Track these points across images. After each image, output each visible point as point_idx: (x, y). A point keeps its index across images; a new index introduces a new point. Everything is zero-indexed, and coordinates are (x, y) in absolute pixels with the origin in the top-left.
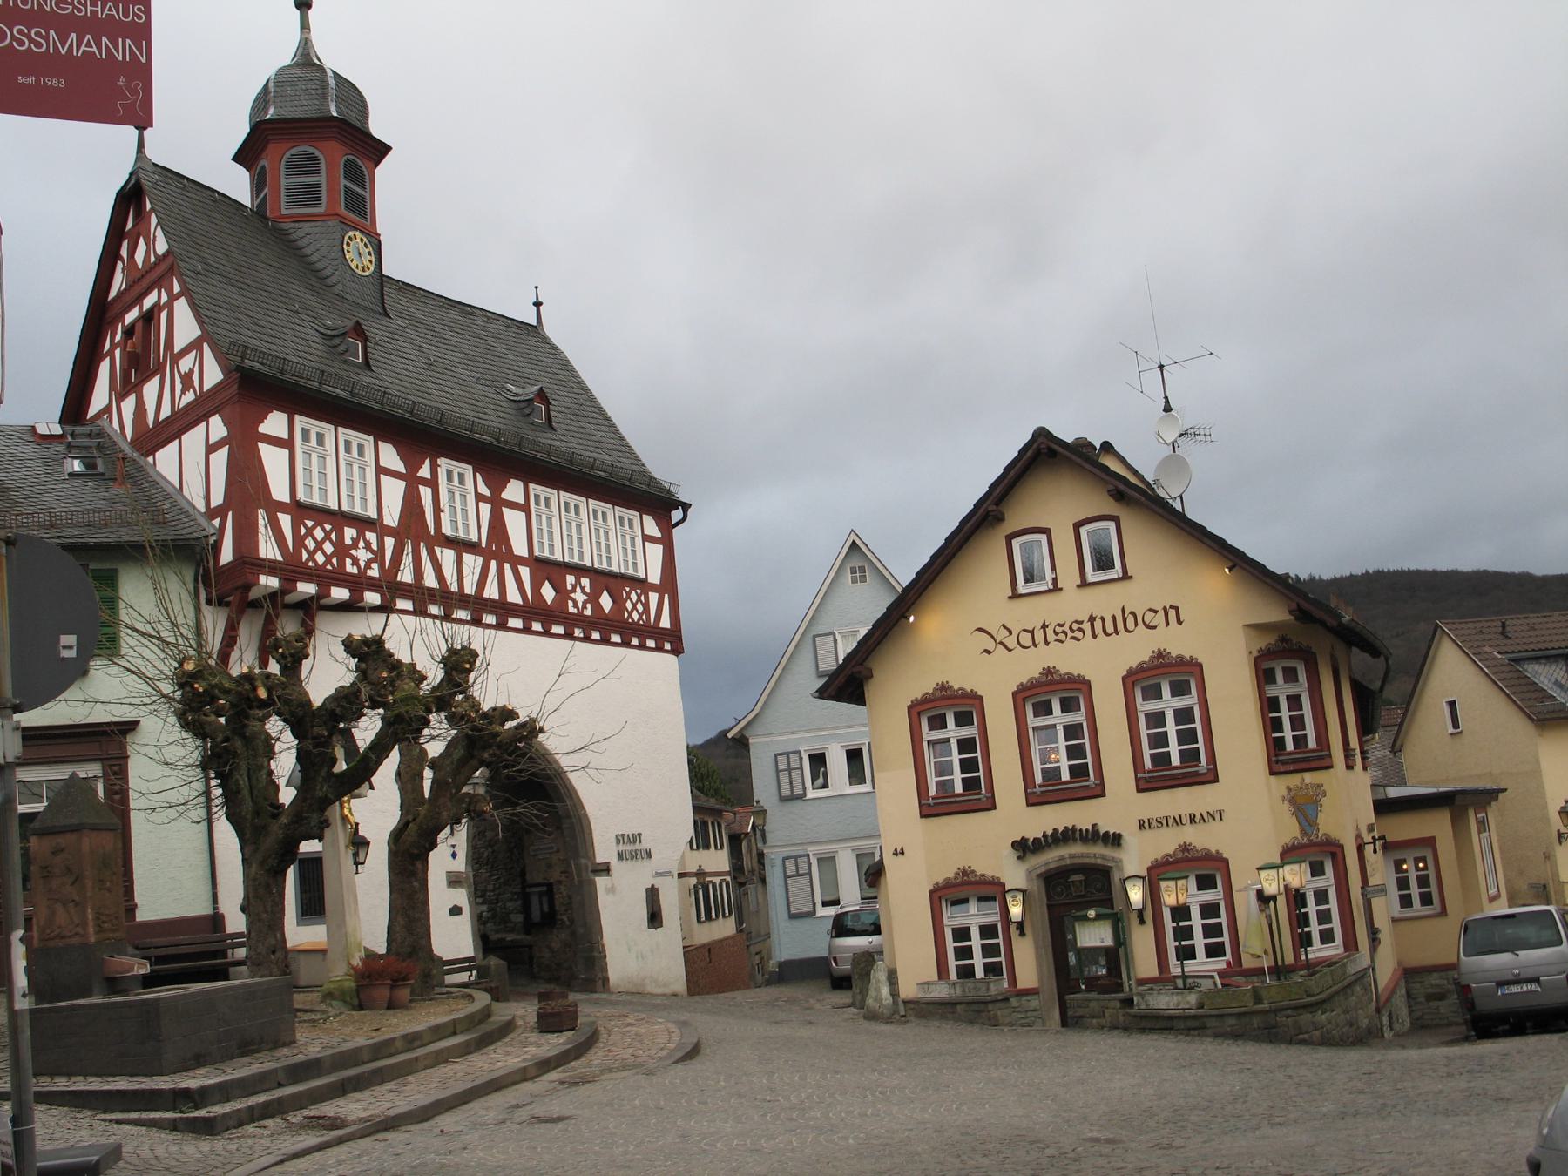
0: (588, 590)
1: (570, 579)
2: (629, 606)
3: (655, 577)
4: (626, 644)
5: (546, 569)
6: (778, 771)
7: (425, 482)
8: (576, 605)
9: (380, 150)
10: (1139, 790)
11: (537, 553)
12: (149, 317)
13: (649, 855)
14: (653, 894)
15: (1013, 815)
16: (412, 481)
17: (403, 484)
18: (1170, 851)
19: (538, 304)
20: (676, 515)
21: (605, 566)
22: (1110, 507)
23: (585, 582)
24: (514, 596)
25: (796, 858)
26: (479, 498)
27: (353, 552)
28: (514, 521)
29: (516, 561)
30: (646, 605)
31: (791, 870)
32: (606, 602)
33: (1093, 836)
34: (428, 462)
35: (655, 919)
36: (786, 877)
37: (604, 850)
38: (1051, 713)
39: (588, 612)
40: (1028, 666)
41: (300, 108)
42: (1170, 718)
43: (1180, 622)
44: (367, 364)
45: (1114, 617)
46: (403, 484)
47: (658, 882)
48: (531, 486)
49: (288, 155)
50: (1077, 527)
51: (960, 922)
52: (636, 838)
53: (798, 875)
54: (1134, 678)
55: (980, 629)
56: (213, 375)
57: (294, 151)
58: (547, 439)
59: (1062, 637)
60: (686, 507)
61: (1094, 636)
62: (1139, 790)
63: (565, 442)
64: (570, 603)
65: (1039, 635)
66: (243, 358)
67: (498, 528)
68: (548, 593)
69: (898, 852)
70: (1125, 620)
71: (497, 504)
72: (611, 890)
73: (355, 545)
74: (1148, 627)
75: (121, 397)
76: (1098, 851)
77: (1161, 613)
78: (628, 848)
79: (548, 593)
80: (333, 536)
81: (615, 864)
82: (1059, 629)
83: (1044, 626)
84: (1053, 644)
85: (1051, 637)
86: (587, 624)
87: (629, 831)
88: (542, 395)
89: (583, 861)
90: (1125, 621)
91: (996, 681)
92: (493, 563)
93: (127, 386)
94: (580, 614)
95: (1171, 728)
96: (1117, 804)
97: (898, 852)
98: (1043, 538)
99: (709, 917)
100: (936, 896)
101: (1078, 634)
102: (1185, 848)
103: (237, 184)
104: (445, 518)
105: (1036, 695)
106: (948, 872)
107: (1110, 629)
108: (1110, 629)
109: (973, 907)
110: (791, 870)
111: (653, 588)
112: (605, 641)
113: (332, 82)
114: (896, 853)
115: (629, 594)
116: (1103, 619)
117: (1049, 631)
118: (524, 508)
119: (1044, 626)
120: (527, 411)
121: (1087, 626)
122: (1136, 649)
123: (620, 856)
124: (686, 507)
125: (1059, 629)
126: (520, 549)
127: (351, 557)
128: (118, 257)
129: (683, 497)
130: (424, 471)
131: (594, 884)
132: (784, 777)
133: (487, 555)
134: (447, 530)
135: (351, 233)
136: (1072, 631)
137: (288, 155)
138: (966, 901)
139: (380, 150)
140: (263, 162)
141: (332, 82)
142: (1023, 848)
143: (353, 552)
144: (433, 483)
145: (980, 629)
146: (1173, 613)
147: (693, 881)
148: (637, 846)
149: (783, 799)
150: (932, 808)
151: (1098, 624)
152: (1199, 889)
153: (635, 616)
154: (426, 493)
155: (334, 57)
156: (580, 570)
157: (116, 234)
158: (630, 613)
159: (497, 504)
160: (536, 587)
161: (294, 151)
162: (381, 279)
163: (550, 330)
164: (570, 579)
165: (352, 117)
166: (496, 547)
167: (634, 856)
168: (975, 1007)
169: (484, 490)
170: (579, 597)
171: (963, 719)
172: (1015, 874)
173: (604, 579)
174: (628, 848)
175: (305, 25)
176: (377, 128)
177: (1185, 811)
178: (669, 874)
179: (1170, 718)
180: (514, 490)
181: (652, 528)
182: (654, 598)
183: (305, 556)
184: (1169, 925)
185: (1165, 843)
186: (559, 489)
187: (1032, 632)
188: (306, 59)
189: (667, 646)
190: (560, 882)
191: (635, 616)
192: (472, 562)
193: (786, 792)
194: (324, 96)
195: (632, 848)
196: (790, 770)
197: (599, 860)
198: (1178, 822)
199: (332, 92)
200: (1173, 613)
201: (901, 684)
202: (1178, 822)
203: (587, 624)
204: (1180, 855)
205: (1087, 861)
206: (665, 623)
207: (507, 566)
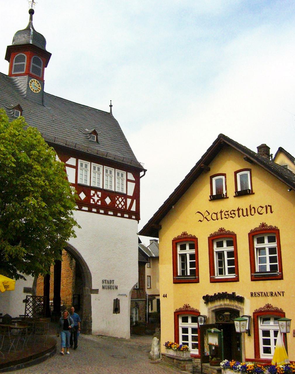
1: (93, 192)
2: (118, 202)
3: (130, 193)
8: (94, 200)
10: (252, 280)
11: (79, 182)
13: (117, 288)
15: (206, 287)
18: (262, 306)
19: (111, 106)
20: (142, 173)
22: (248, 165)
23: (99, 194)
27: (93, 197)
30: (126, 204)
32: (108, 201)
33: (233, 297)
35: (116, 310)
38: (223, 246)
40: (214, 227)
43: (271, 212)
45: (247, 209)
47: (119, 298)
48: (79, 160)
50: (236, 173)
51: (266, 328)
52: (112, 281)
54: (253, 234)
55: (198, 212)
59: (227, 216)
60: (145, 171)
61: (239, 216)
62: (252, 280)
63: (105, 148)
64: (92, 200)
65: (219, 215)
69: (165, 296)
70: (251, 210)
73: (94, 195)
74: (259, 213)
76: (234, 305)
77: (265, 208)
79: (83, 196)
80: (124, 200)
81: (100, 289)
82: (226, 213)
83: (221, 212)
84: (224, 219)
85: (223, 216)
87: (108, 279)
88: (95, 132)
90: (251, 211)
91: (202, 233)
94: (96, 204)
96: (244, 286)
97: (165, 296)
98: (223, 177)
100: (176, 314)
101: (233, 215)
102: (268, 306)
105: (217, 238)
106: (180, 306)
107: (245, 214)
108: (245, 214)
109: (272, 323)
111: (130, 197)
114: (164, 296)
115: (118, 199)
116: (242, 210)
117: (223, 214)
118: (76, 167)
119: (221, 212)
121: (236, 212)
122: (254, 222)
123: (103, 288)
124: (145, 171)
125: (226, 213)
129: (145, 168)
131: (90, 296)
135: (33, 80)
136: (231, 214)
137: (16, 56)
138: (268, 319)
142: (208, 299)
145: (198, 212)
146: (269, 208)
148: (112, 284)
150: (177, 280)
151: (241, 212)
152: (192, 322)
156: (96, 189)
158: (118, 205)
161: (18, 55)
163: (114, 114)
164: (93, 192)
167: (110, 288)
168: (178, 361)
172: (204, 310)
173: (106, 193)
174: (108, 285)
175: (31, 19)
176: (48, 49)
177: (269, 291)
180: (72, 161)
181: (131, 177)
182: (129, 201)
183: (116, 205)
184: (261, 338)
185: (260, 303)
186: (103, 165)
187: (217, 214)
195: (109, 285)
197: (94, 287)
198: (266, 295)
200: (269, 208)
201: (173, 230)
202: (266, 295)
203: (98, 208)
204: (266, 309)
205: (230, 307)
206: (133, 209)
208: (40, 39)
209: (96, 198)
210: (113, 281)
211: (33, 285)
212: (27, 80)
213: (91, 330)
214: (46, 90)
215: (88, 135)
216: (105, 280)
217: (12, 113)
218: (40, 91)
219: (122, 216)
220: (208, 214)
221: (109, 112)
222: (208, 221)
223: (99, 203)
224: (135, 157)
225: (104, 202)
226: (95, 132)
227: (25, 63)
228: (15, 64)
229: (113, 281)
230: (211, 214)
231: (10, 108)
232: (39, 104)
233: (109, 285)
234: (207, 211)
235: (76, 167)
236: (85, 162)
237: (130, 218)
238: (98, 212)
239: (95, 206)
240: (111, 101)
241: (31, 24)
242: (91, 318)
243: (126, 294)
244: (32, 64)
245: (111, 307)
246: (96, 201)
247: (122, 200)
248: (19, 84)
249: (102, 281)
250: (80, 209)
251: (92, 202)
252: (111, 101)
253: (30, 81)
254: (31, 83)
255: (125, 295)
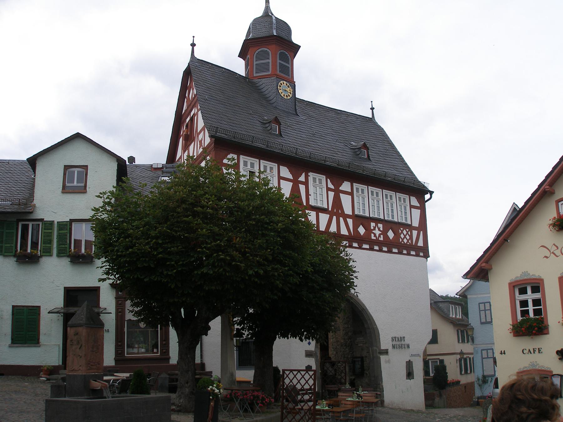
0: (381, 229)
1: (373, 225)
2: (402, 236)
3: (416, 224)
4: (400, 253)
5: (360, 220)
6: (480, 311)
7: (302, 183)
9: (296, 48)
11: (356, 213)
12: (192, 119)
13: (408, 346)
14: (409, 364)
16: (296, 183)
17: (291, 184)
19: (372, 109)
20: (427, 197)
21: (390, 219)
23: (380, 226)
24: (344, 231)
25: (487, 350)
26: (328, 189)
27: (374, 231)
28: (346, 200)
29: (346, 217)
30: (411, 236)
31: (485, 355)
32: (391, 234)
34: (304, 174)
35: (410, 375)
36: (483, 358)
37: (385, 343)
39: (381, 239)
41: (263, 33)
42: (530, 303)
44: (280, 134)
46: (291, 184)
47: (412, 359)
48: (354, 184)
49: (257, 52)
53: (488, 358)
55: (542, 246)
56: (208, 140)
57: (259, 50)
58: (369, 166)
60: (431, 193)
63: (376, 166)
64: (372, 235)
66: (216, 132)
67: (337, 202)
68: (362, 230)
71: (338, 192)
72: (389, 362)
73: (374, 229)
75: (184, 152)
78: (398, 343)
79: (362, 230)
80: (409, 233)
86: (381, 244)
87: (399, 335)
88: (365, 146)
89: (375, 348)
92: (335, 217)
93: (186, 148)
94: (377, 239)
95: (531, 308)
99: (466, 372)
103: (239, 67)
104: (311, 199)
110: (485, 355)
111: (415, 228)
112: (390, 251)
113: (274, 21)
114: (501, 353)
115: (402, 231)
118: (351, 194)
120: (358, 153)
123: (394, 347)
124: (431, 193)
126: (348, 210)
127: (373, 233)
128: (185, 97)
129: (430, 189)
130: (302, 178)
132: (483, 313)
133: (331, 214)
134: (312, 203)
135: (282, 82)
137: (257, 52)
139: (296, 48)
140: (248, 56)
141: (274, 21)
143: (374, 231)
144: (306, 183)
145: (542, 246)
147: (458, 356)
149: (482, 323)
153: (405, 241)
154: (302, 188)
155: (278, 12)
156: (377, 221)
157: (184, 88)
158: (403, 240)
159: (338, 192)
160: (356, 227)
161: (259, 50)
162: (295, 100)
164: (373, 225)
165: (283, 35)
166: (336, 210)
167: (401, 347)
169: (331, 186)
170: (377, 232)
171: (536, 289)
173: (389, 224)
174: (398, 343)
176: (295, 39)
178: (419, 355)
179: (530, 303)
180: (346, 186)
181: (414, 201)
182: (415, 233)
186: (368, 185)
188: (267, 14)
189: (421, 254)
190: (366, 357)
191: (405, 241)
192: (324, 218)
193: (483, 320)
194: (271, 28)
195: (400, 343)
196: (485, 310)
197: (383, 347)
199: (274, 26)
203: (381, 244)
206: (421, 244)
207: (341, 219)
208: (284, 27)
209: (377, 232)
210: (404, 337)
211: (465, 384)
212: (275, 83)
213: (384, 401)
214: (299, 95)
215: (357, 150)
216: (395, 337)
217: (269, 128)
218: (291, 96)
219: (409, 254)
220: (556, 248)
221: (371, 117)
222: (557, 256)
223: (381, 239)
224: (414, 175)
225: (386, 236)
226: (365, 146)
227: (270, 61)
228: (258, 62)
229: (404, 337)
230: (560, 249)
231: (265, 122)
232: (292, 114)
233: (400, 343)
234: (554, 244)
235: (351, 194)
236: (361, 186)
237: (417, 255)
238: (380, 250)
239: (377, 242)
240: (194, 37)
241: (267, 8)
242: (382, 386)
243: (78, 136)
244: (278, 61)
245: (404, 373)
246: (377, 235)
247: (407, 233)
248: (265, 89)
249: (391, 339)
250: (360, 248)
251: (373, 238)
252: (194, 37)
253: (279, 84)
254: (280, 86)
255: (419, 355)
